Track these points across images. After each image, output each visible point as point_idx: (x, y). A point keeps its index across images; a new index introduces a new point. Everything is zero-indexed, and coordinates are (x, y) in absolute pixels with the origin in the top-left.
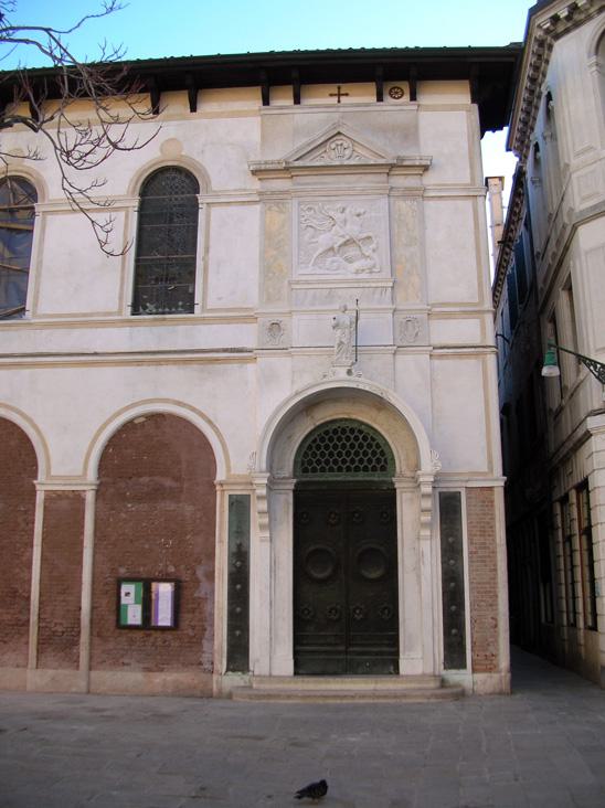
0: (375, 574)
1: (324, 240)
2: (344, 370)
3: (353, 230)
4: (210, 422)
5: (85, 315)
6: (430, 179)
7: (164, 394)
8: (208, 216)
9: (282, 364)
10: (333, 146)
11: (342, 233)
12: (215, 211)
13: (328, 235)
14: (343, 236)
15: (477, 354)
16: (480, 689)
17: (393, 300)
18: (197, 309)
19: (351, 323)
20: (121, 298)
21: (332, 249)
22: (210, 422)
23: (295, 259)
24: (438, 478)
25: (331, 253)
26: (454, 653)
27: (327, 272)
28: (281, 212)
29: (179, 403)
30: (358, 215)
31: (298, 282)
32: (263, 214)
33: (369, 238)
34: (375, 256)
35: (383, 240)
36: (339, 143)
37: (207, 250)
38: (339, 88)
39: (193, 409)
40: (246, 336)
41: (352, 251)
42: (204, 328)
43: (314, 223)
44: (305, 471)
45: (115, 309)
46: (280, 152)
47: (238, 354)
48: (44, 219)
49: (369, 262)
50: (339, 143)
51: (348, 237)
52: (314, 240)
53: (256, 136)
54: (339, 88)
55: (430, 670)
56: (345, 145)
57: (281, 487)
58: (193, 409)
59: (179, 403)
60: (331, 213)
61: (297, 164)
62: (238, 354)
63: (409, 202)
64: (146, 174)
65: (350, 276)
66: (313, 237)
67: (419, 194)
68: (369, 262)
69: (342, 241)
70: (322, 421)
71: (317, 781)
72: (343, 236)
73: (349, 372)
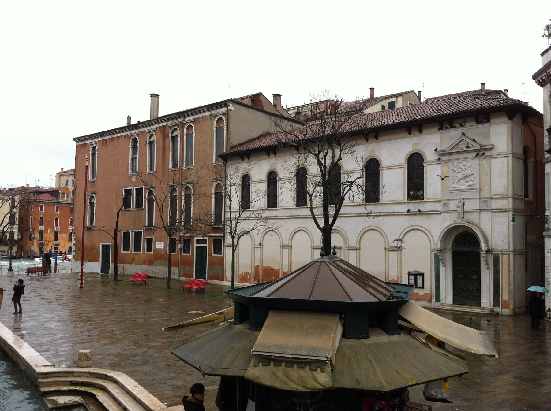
0: (475, 277)
1: (460, 176)
2: (460, 220)
3: (468, 172)
4: (429, 232)
5: (395, 201)
6: (493, 152)
7: (417, 224)
8: (426, 168)
9: (447, 215)
10: (461, 144)
11: (464, 173)
12: (428, 167)
13: (461, 174)
14: (464, 175)
15: (506, 211)
16: (504, 313)
17: (480, 194)
18: (424, 198)
19: (462, 206)
20: (404, 196)
21: (462, 178)
22: (429, 232)
23: (451, 182)
24: (230, 105)
25: (461, 180)
26: (496, 302)
27: (461, 186)
28: (447, 167)
29: (421, 226)
30: (470, 167)
31: (451, 190)
32: (442, 168)
33: (473, 174)
34: (474, 180)
35: (477, 175)
36: (463, 142)
37: (427, 180)
38: (465, 120)
39: (424, 228)
40: (438, 207)
41: (467, 179)
42: (427, 205)
43: (456, 170)
44: (456, 246)
45: (403, 199)
46: (445, 146)
47: (437, 213)
48: (382, 172)
49: (473, 183)
50: (463, 142)
51: (466, 175)
52: (456, 176)
53: (439, 140)
54: (465, 120)
55: (489, 307)
56: (465, 143)
57: (447, 251)
58: (424, 228)
59: (421, 226)
60: (461, 166)
61: (450, 151)
62: (437, 213)
63: (486, 161)
64: (409, 155)
65: (467, 188)
66: (456, 175)
67: (490, 157)
68: (473, 183)
69: (464, 176)
70: (459, 232)
71: (412, 90)
72: (464, 175)
73: (461, 220)
